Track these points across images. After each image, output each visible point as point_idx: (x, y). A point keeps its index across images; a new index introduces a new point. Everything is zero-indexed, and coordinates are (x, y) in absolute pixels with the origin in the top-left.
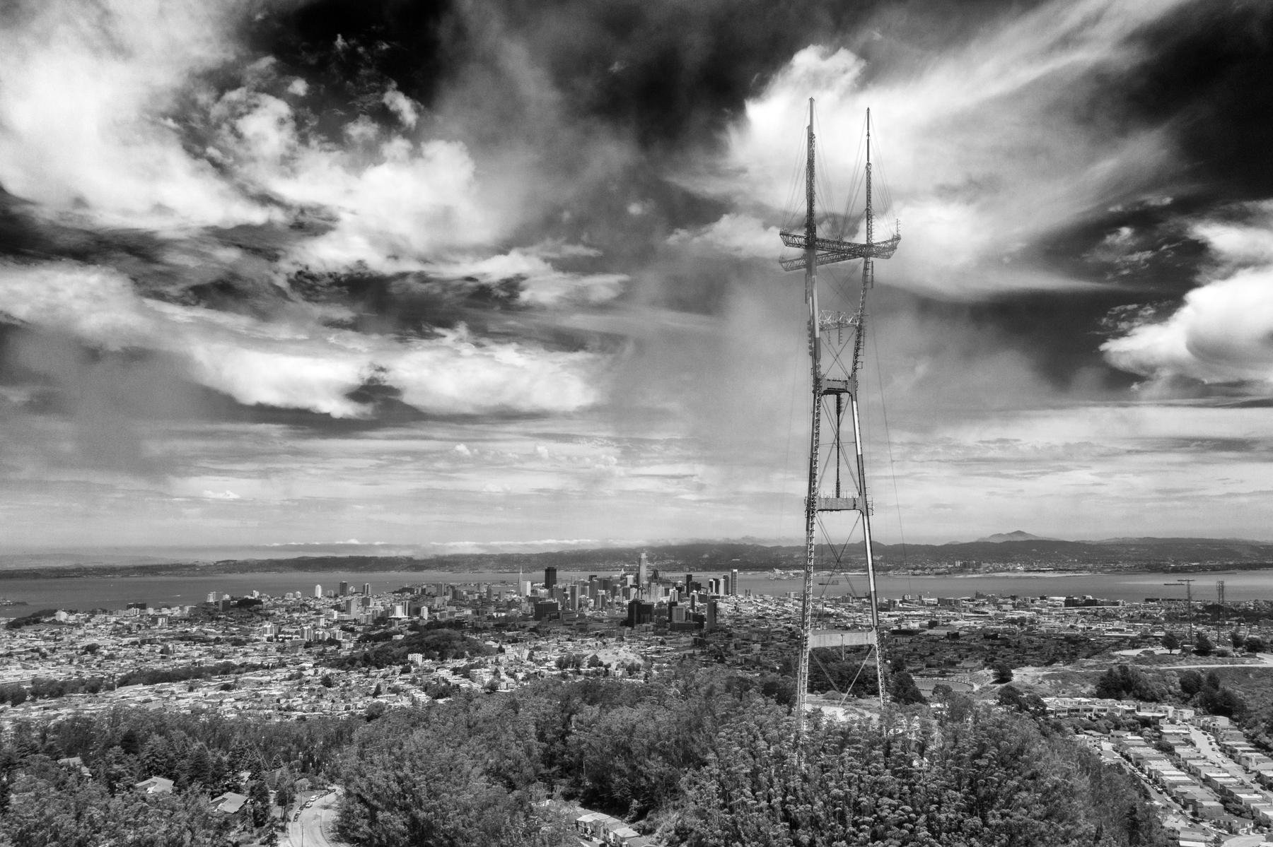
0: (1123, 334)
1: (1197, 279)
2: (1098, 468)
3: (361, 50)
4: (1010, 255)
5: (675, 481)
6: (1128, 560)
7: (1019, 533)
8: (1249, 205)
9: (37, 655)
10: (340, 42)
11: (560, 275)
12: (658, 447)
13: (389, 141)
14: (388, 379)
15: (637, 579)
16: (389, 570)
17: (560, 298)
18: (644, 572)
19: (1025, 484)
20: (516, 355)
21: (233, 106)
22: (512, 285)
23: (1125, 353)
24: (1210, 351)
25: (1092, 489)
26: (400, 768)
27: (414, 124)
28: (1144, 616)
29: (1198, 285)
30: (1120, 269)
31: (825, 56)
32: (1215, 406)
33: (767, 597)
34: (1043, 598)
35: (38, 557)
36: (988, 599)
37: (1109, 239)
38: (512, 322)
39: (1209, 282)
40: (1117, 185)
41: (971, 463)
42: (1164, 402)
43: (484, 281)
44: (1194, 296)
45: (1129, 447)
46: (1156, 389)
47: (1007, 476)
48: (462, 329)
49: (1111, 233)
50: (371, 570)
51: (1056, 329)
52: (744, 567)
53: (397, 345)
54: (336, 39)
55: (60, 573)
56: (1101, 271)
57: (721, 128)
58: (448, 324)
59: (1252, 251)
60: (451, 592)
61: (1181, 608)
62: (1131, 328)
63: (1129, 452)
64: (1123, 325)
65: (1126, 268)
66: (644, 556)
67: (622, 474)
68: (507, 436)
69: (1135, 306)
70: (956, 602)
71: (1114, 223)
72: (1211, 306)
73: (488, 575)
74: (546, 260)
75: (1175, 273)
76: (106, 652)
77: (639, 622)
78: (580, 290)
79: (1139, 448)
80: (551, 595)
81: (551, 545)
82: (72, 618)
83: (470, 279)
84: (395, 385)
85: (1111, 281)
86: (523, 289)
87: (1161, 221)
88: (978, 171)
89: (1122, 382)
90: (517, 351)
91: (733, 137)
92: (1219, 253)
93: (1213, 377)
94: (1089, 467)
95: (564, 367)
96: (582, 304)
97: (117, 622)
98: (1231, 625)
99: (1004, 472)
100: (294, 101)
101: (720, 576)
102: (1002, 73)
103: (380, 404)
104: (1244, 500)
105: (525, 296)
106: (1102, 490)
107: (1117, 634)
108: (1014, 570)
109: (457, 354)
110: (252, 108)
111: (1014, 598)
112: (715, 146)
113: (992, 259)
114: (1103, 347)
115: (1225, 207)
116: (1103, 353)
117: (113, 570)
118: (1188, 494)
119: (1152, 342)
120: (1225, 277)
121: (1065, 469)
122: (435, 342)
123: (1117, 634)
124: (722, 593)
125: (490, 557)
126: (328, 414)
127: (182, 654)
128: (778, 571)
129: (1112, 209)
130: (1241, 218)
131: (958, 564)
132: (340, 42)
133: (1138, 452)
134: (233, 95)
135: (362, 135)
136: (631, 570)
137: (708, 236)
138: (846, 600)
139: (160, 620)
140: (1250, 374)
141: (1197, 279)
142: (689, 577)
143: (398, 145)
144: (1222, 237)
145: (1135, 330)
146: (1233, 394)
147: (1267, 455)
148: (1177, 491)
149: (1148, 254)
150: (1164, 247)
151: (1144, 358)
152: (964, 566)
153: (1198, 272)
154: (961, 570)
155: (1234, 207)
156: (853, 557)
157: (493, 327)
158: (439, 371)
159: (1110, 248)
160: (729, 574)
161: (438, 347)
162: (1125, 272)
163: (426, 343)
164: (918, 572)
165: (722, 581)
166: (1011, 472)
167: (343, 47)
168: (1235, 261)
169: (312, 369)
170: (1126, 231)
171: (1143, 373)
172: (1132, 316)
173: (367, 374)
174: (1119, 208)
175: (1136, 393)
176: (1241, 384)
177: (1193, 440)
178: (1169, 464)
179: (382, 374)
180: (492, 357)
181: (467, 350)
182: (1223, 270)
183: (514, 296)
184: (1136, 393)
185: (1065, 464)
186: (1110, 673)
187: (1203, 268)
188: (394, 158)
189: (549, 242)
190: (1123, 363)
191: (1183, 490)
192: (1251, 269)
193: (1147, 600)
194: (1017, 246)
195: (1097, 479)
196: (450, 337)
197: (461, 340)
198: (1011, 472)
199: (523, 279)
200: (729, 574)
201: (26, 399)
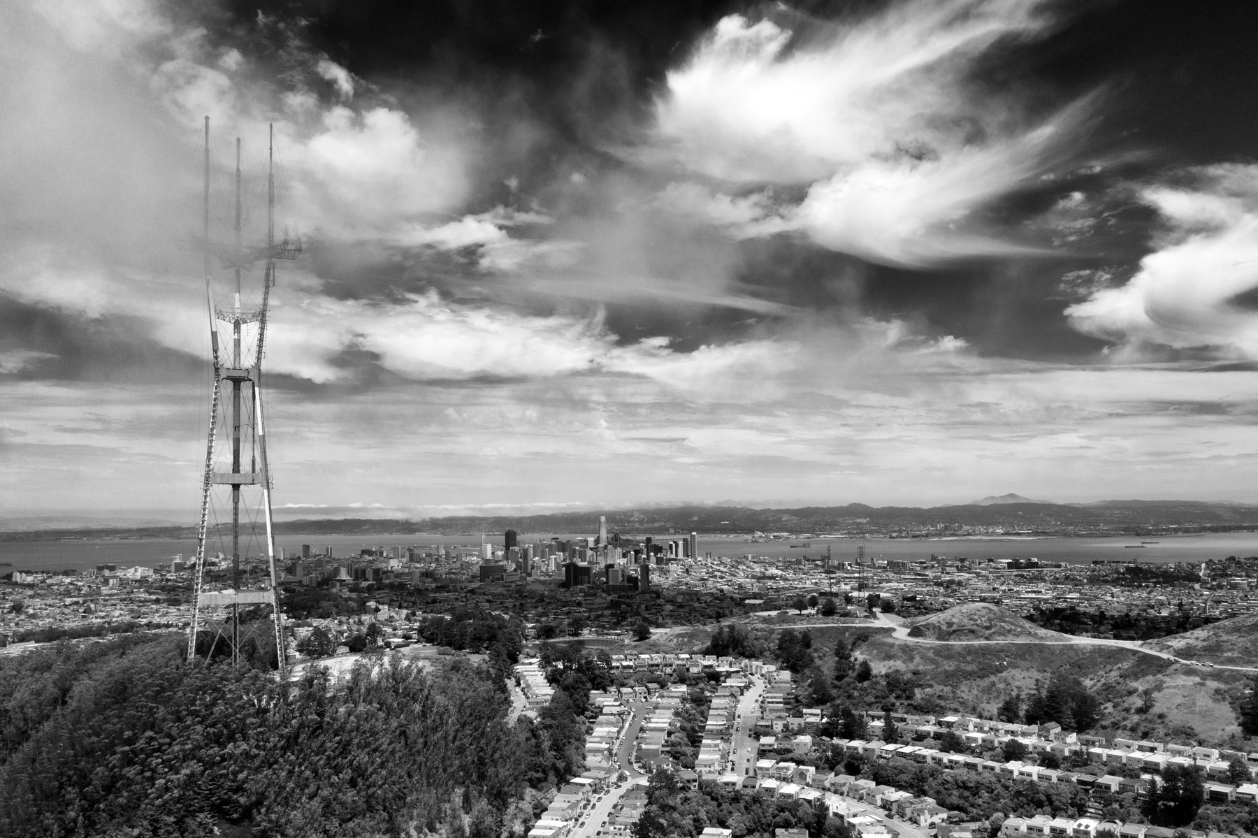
0: (1082, 300)
1: (1151, 244)
2: (1085, 431)
3: (281, 25)
4: (953, 221)
5: (667, 444)
6: (1112, 522)
7: (1012, 495)
8: (1195, 170)
9: (954, 587)
10: (261, 17)
11: (515, 242)
12: (643, 411)
13: (329, 110)
14: (369, 344)
15: (597, 541)
16: (381, 533)
17: (521, 265)
18: (604, 534)
19: (1017, 448)
20: (487, 321)
21: (171, 79)
22: (472, 253)
23: (1089, 318)
24: (1167, 316)
25: (1081, 452)
26: (193, 704)
27: (351, 93)
28: (1067, 578)
29: (1152, 251)
30: (1066, 236)
31: (749, 26)
32: (1180, 370)
33: (724, 559)
34: (990, 560)
35: (49, 520)
36: (938, 562)
37: (1062, 204)
38: (478, 289)
39: (1162, 248)
40: (1049, 155)
41: (963, 423)
42: (1132, 366)
43: (443, 248)
44: (1149, 261)
45: (1109, 411)
46: (1127, 353)
47: (997, 439)
48: (433, 296)
49: (1063, 198)
50: (366, 532)
51: (990, 302)
52: (703, 530)
53: (370, 312)
54: (257, 15)
55: (38, 536)
56: (1045, 238)
57: (647, 100)
58: (420, 290)
59: (1202, 217)
60: (407, 554)
61: (1103, 570)
62: (1091, 293)
63: (1110, 415)
64: (1082, 291)
65: (1071, 234)
66: (603, 519)
67: (613, 438)
68: (494, 400)
69: (1088, 272)
70: (904, 564)
71: (1062, 189)
72: (1164, 270)
73: (456, 538)
74: (501, 228)
75: (1129, 239)
76: (31, 611)
77: (576, 584)
78: (540, 257)
79: (1120, 411)
80: (506, 557)
81: (543, 508)
82: (30, 579)
83: (429, 246)
84: (375, 350)
85: (1060, 246)
86: (482, 256)
87: (1108, 187)
88: (908, 140)
89: (1089, 348)
90: (488, 316)
91: (660, 108)
92: (1169, 219)
93: (1177, 342)
94: (1075, 431)
95: (537, 332)
96: (539, 268)
97: (71, 583)
98: (1147, 586)
99: (993, 435)
100: (232, 75)
101: (680, 539)
102: (922, 41)
103: (363, 370)
104: (1232, 462)
105: (485, 263)
106: (1090, 453)
107: (1033, 595)
108: (993, 533)
109: (430, 320)
110: (191, 80)
111: (962, 560)
112: (643, 116)
113: (941, 228)
114: (1067, 312)
115: (1171, 173)
116: (1067, 317)
117: (114, 532)
118: (1175, 457)
119: (1110, 306)
120: (1178, 242)
121: (1053, 433)
122: (407, 308)
123: (1033, 595)
124: (681, 556)
125: (481, 520)
126: (309, 380)
127: (103, 614)
128: (758, 534)
129: (1044, 177)
130: (1190, 184)
131: (940, 526)
132: (261, 17)
133: (1119, 415)
134: (168, 66)
135: (302, 105)
136: (593, 532)
137: (656, 204)
138: (799, 562)
139: (111, 581)
140: (1213, 340)
141: (1151, 244)
142: (649, 540)
143: (339, 115)
144: (1172, 202)
145: (1096, 295)
146: (1202, 358)
147: (1250, 418)
148: (1165, 454)
149: (1090, 222)
150: (1106, 214)
151: (1107, 323)
152: (946, 528)
153: (1151, 237)
154: (940, 534)
155: (1181, 173)
156: (840, 520)
157: (459, 293)
158: (423, 337)
159: (1065, 213)
160: (688, 537)
161: (408, 313)
162: (1072, 238)
163: (399, 308)
164: (894, 535)
165: (681, 543)
166: (998, 435)
167: (265, 24)
168: (1186, 226)
169: (297, 336)
170: (1077, 196)
171: (1112, 339)
172: (1088, 282)
173: (347, 339)
174: (1052, 176)
175: (1107, 356)
176: (1206, 348)
177: (1172, 403)
178: (1155, 427)
179: (360, 339)
180: (465, 322)
181: (443, 315)
182: (1174, 235)
183: (474, 263)
184: (1107, 356)
185: (1051, 427)
186: (721, 632)
187: (1156, 234)
188: (336, 127)
189: (501, 210)
190: (1085, 327)
191: (1173, 453)
192: (1203, 234)
193: (1095, 563)
194: (961, 213)
195: (1084, 442)
196: (422, 302)
197: (432, 305)
198: (998, 435)
199: (482, 246)
200: (688, 537)
201: (21, 366)
